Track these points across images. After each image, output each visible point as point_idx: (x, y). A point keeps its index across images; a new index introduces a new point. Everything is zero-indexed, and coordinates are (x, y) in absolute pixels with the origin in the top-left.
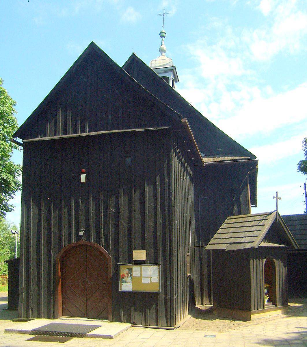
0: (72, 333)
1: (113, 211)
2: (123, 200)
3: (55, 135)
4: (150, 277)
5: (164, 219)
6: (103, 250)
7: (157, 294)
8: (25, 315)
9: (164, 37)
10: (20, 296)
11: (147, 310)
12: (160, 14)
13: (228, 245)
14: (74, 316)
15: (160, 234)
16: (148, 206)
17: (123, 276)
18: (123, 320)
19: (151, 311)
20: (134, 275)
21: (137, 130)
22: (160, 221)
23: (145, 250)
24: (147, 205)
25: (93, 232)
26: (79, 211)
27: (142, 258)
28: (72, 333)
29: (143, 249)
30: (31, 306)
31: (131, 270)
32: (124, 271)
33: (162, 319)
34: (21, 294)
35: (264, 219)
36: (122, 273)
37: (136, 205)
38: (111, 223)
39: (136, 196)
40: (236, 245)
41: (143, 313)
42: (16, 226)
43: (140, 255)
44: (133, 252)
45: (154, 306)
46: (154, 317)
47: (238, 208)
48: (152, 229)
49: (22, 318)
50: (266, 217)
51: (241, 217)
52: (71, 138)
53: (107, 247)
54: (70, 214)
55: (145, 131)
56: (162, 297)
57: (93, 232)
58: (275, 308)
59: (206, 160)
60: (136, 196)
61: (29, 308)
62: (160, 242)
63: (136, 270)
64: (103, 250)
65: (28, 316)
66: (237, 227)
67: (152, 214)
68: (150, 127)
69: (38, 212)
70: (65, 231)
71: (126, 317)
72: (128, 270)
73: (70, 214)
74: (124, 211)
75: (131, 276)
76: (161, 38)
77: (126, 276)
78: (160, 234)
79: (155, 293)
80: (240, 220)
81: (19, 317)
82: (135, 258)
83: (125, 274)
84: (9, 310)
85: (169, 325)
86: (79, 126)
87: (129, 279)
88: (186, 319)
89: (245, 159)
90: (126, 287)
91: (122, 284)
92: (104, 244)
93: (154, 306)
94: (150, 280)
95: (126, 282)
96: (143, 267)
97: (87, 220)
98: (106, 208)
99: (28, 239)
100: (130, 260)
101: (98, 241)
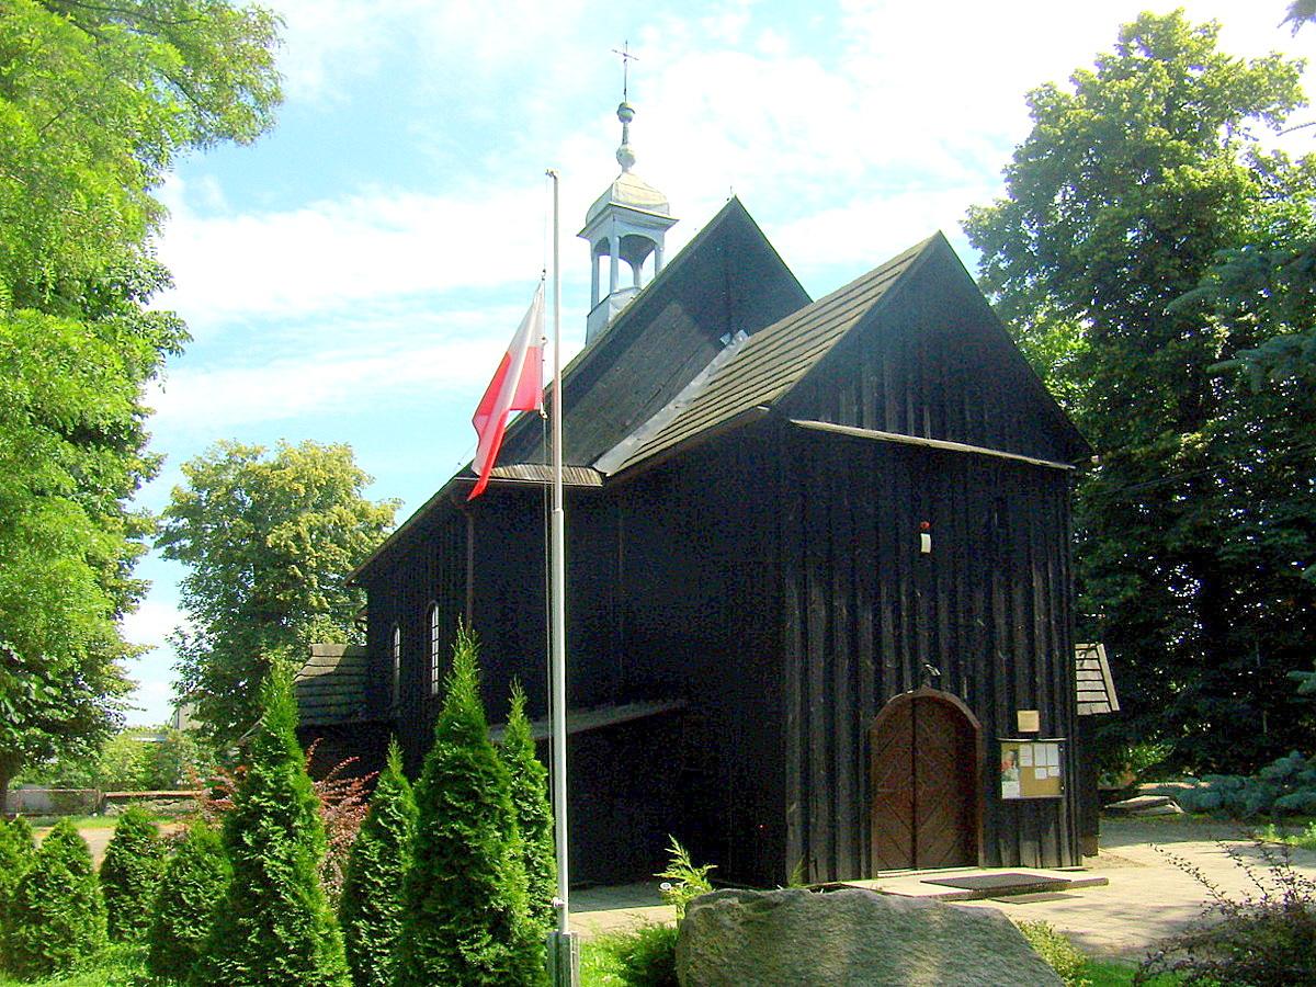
4: (1047, 767)
7: (1057, 801)
10: (790, 828)
21: (1031, 460)
33: (1067, 858)
43: (1029, 720)
63: (1025, 750)
65: (834, 874)
75: (1018, 765)
100: (1014, 732)
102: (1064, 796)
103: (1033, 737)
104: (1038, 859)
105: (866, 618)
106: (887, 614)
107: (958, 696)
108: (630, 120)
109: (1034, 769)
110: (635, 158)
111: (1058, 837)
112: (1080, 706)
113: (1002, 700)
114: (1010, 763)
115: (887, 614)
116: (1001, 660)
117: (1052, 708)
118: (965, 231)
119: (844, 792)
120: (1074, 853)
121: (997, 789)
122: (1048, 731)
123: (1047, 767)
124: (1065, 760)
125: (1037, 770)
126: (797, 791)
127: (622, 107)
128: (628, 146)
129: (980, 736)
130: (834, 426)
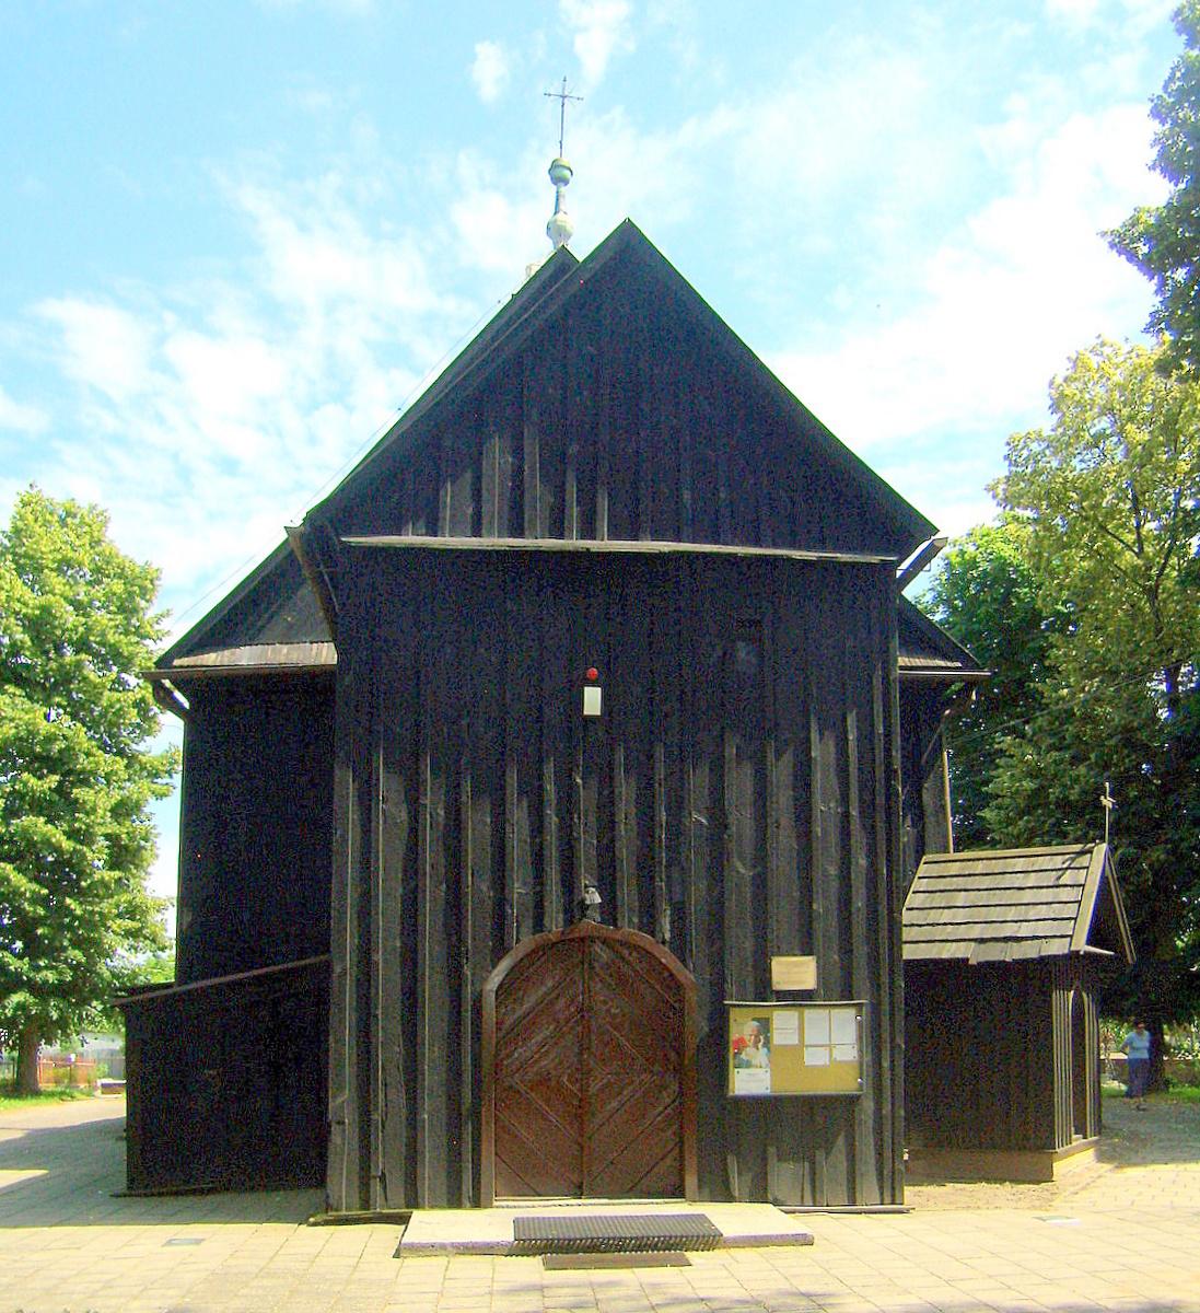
0: (671, 1237)
1: (701, 824)
2: (740, 782)
3: (477, 533)
4: (830, 1047)
5: (872, 853)
6: (667, 957)
7: (851, 1101)
8: (356, 1200)
9: (566, 182)
10: (335, 1128)
11: (820, 1155)
12: (550, 95)
13: (973, 944)
14: (540, 1195)
15: (859, 903)
16: (821, 811)
17: (740, 1044)
18: (737, 1195)
19: (831, 1157)
20: (778, 1038)
21: (797, 554)
22: (861, 861)
23: (811, 958)
24: (819, 806)
25: (628, 893)
26: (576, 816)
27: (804, 982)
28: (671, 1237)
29: (810, 954)
30: (379, 1164)
31: (765, 1026)
32: (742, 1026)
33: (869, 1186)
34: (338, 1123)
35: (1067, 869)
36: (734, 1035)
37: (783, 800)
38: (697, 862)
39: (781, 772)
40: (1003, 944)
41: (807, 1164)
42: (149, 870)
43: (795, 971)
44: (773, 963)
45: (841, 1141)
46: (843, 1177)
47: (914, 825)
48: (835, 885)
49: (344, 1213)
50: (1073, 860)
51: (966, 857)
52: (537, 555)
53: (680, 947)
54: (538, 828)
55: (820, 561)
56: (868, 1105)
57: (628, 893)
58: (1084, 1144)
59: (903, 661)
60: (781, 772)
61: (373, 1173)
62: (859, 928)
63: (784, 1022)
64: (667, 957)
65: (367, 1202)
66: (979, 890)
67: (834, 838)
68: (793, 545)
69: (404, 816)
70: (519, 889)
71: (748, 1177)
72: (756, 1023)
73: (538, 828)
74: (741, 820)
75: (767, 1043)
76: (555, 184)
77: (751, 1044)
78: (859, 903)
79: (847, 1097)
80: (980, 867)
81: (328, 1207)
82: (778, 983)
83: (747, 1038)
84: (131, 1195)
85: (888, 1199)
86: (574, 511)
87: (759, 1055)
88: (1076, 1162)
89: (942, 668)
90: (750, 1080)
91: (736, 1070)
92: (667, 936)
93: (841, 1141)
94: (831, 1056)
95: (748, 1065)
96: (807, 1012)
97: (607, 850)
98: (678, 806)
99: (415, 917)
100: (763, 989)
101: (650, 925)
102: (868, 1092)
103: (799, 998)
104: (807, 1187)
105: (477, 824)
106: (519, 815)
107: (652, 934)
108: (566, 182)
109: (806, 1045)
110: (568, 228)
111: (852, 1157)
112: (906, 947)
113: (741, 939)
114: (749, 1040)
115: (519, 815)
116: (742, 877)
117: (847, 951)
118: (1112, 245)
119: (432, 1076)
120: (887, 1185)
121: (722, 1079)
122: (836, 988)
123: (830, 1047)
124: (873, 1037)
125: (807, 1052)
126: (349, 1071)
127: (555, 166)
128: (560, 216)
129: (692, 997)
130: (475, 540)
